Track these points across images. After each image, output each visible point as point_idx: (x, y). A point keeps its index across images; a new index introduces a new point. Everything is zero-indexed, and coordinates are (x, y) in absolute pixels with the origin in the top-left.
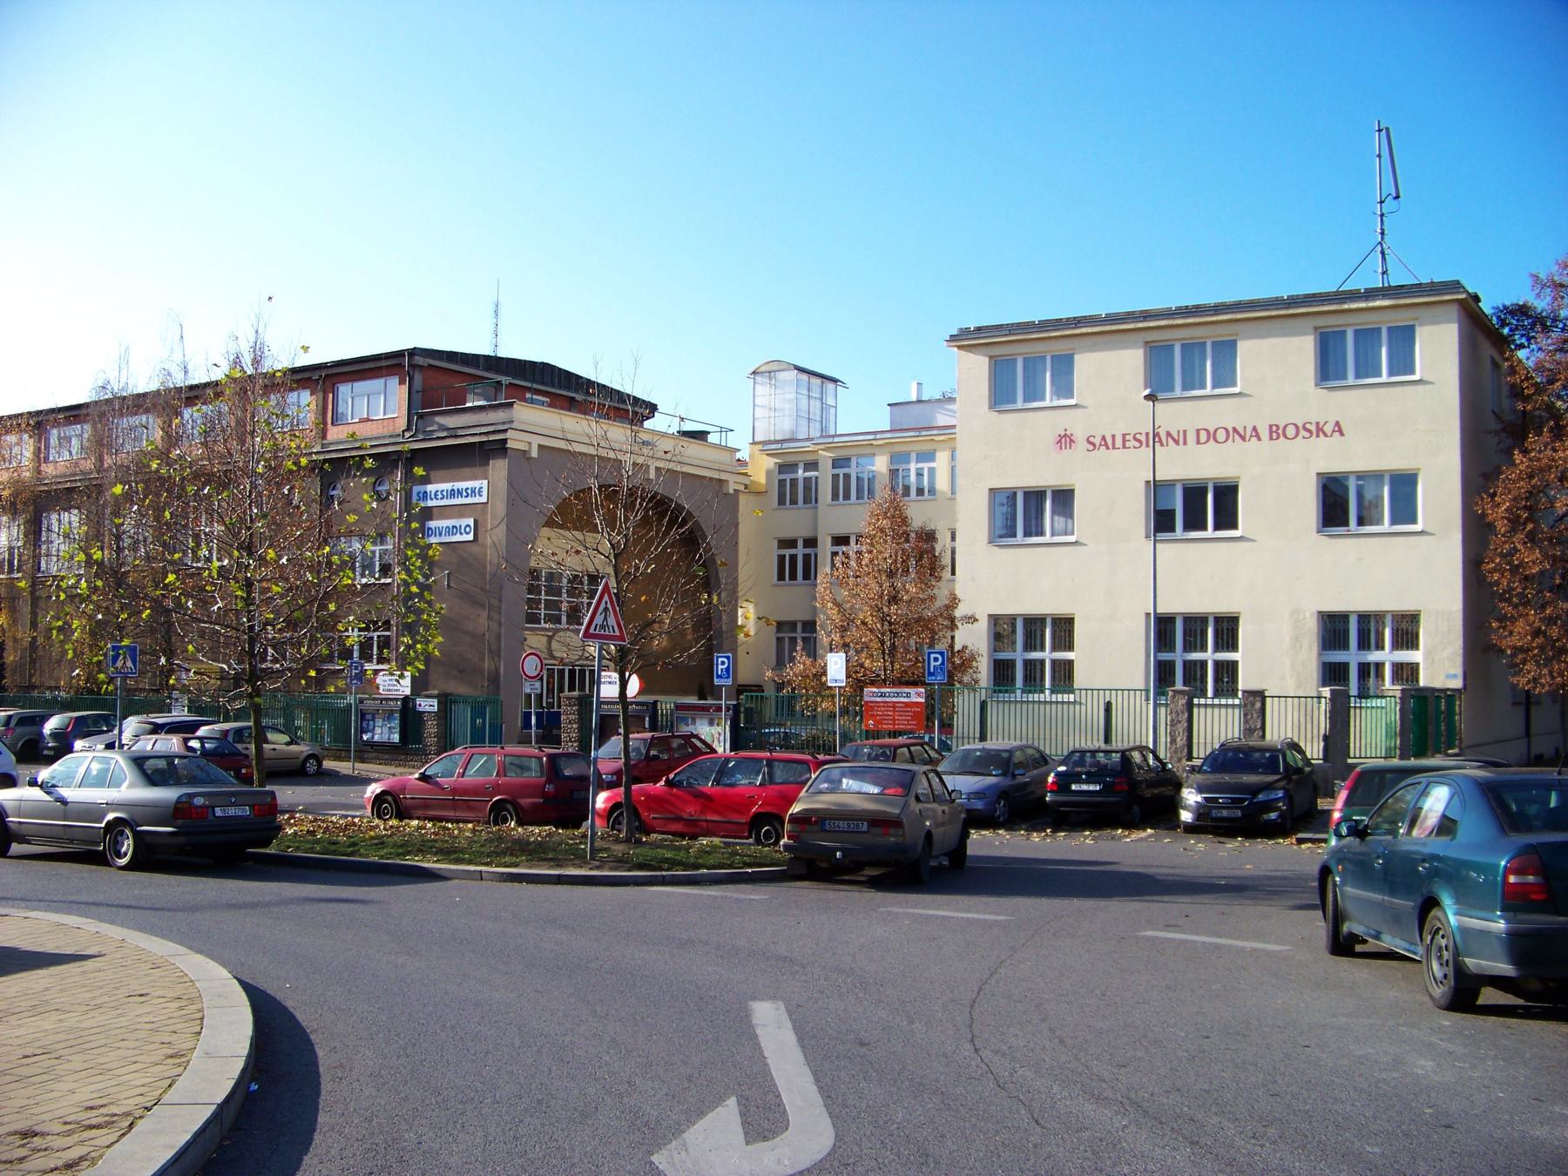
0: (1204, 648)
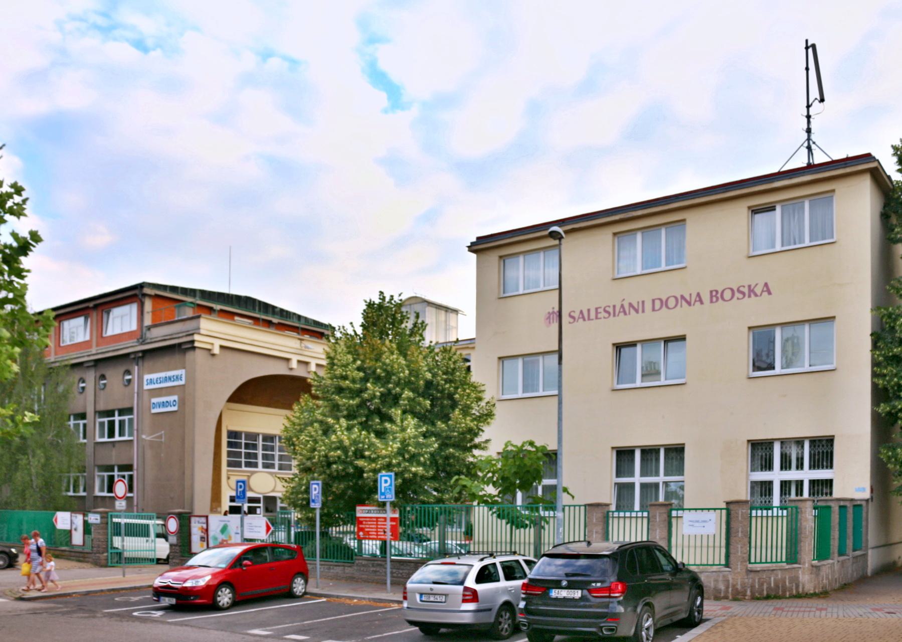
0: (632, 474)
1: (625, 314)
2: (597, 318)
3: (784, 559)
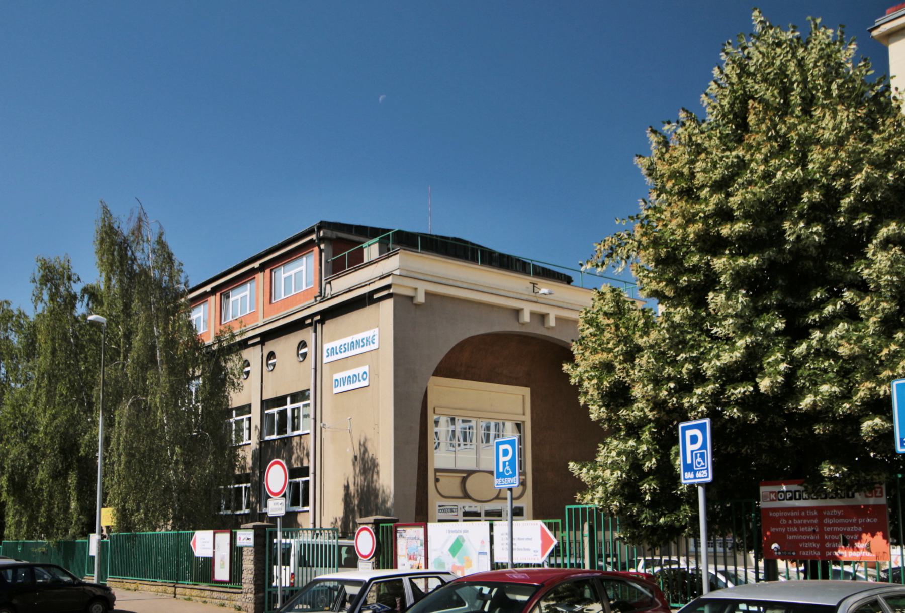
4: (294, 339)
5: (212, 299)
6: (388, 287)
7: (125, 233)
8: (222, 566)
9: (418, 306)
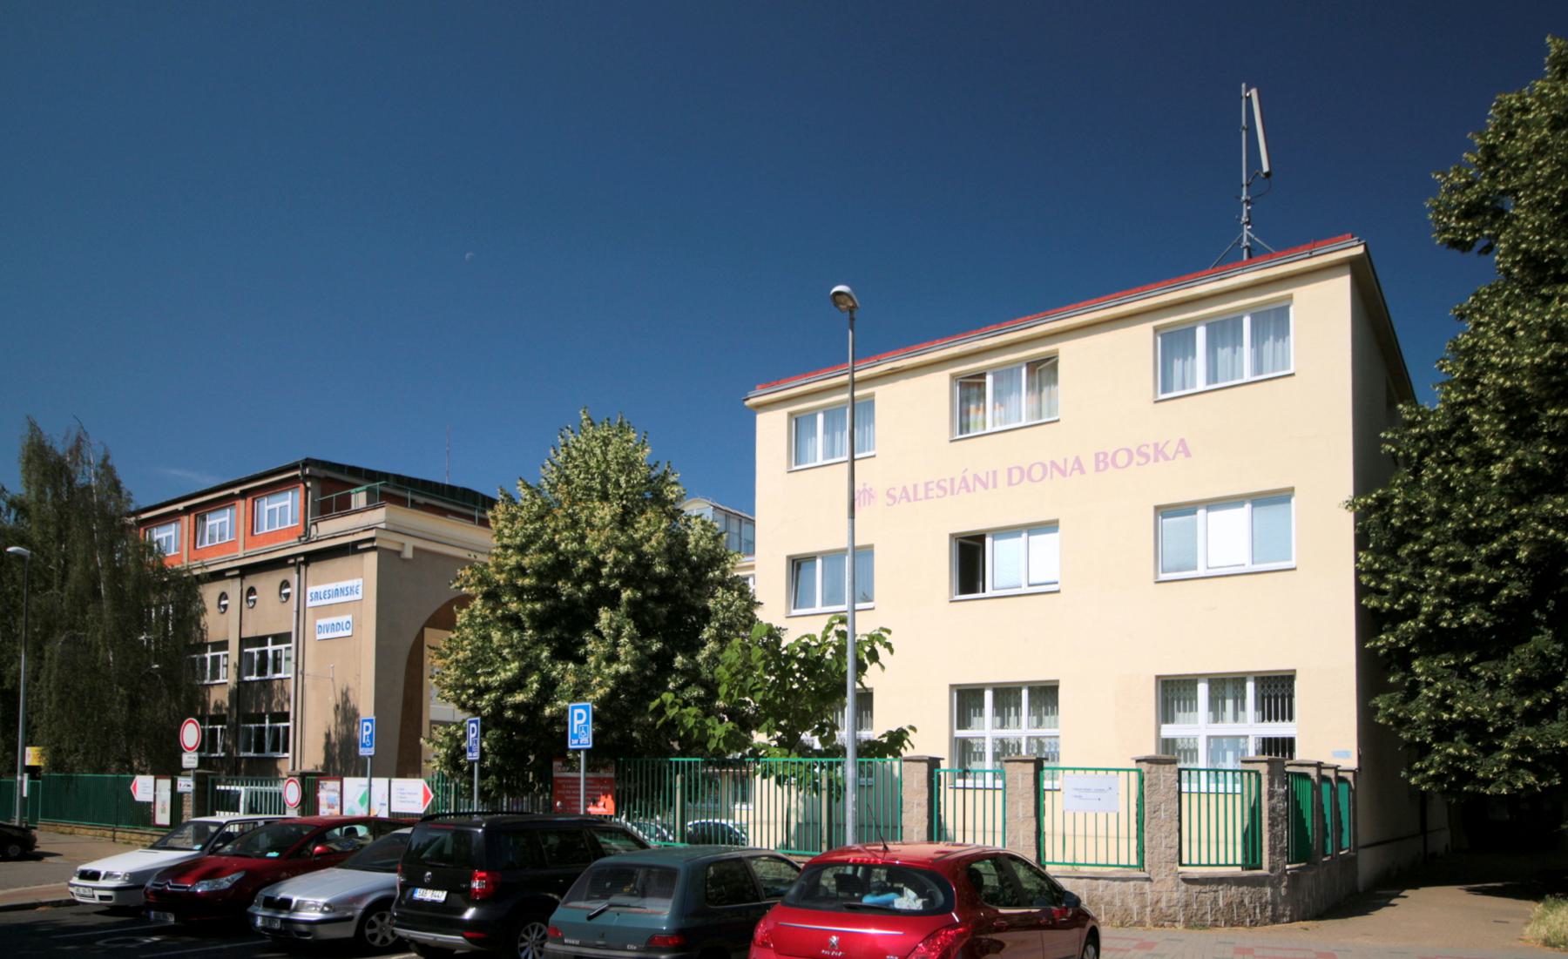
1: (968, 491)
2: (927, 497)
3: (1239, 861)
4: (277, 577)
5: (185, 519)
6: (372, 540)
7: (60, 451)
8: (163, 811)
9: (406, 560)
